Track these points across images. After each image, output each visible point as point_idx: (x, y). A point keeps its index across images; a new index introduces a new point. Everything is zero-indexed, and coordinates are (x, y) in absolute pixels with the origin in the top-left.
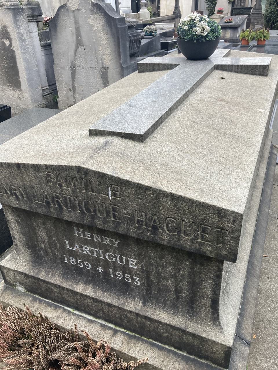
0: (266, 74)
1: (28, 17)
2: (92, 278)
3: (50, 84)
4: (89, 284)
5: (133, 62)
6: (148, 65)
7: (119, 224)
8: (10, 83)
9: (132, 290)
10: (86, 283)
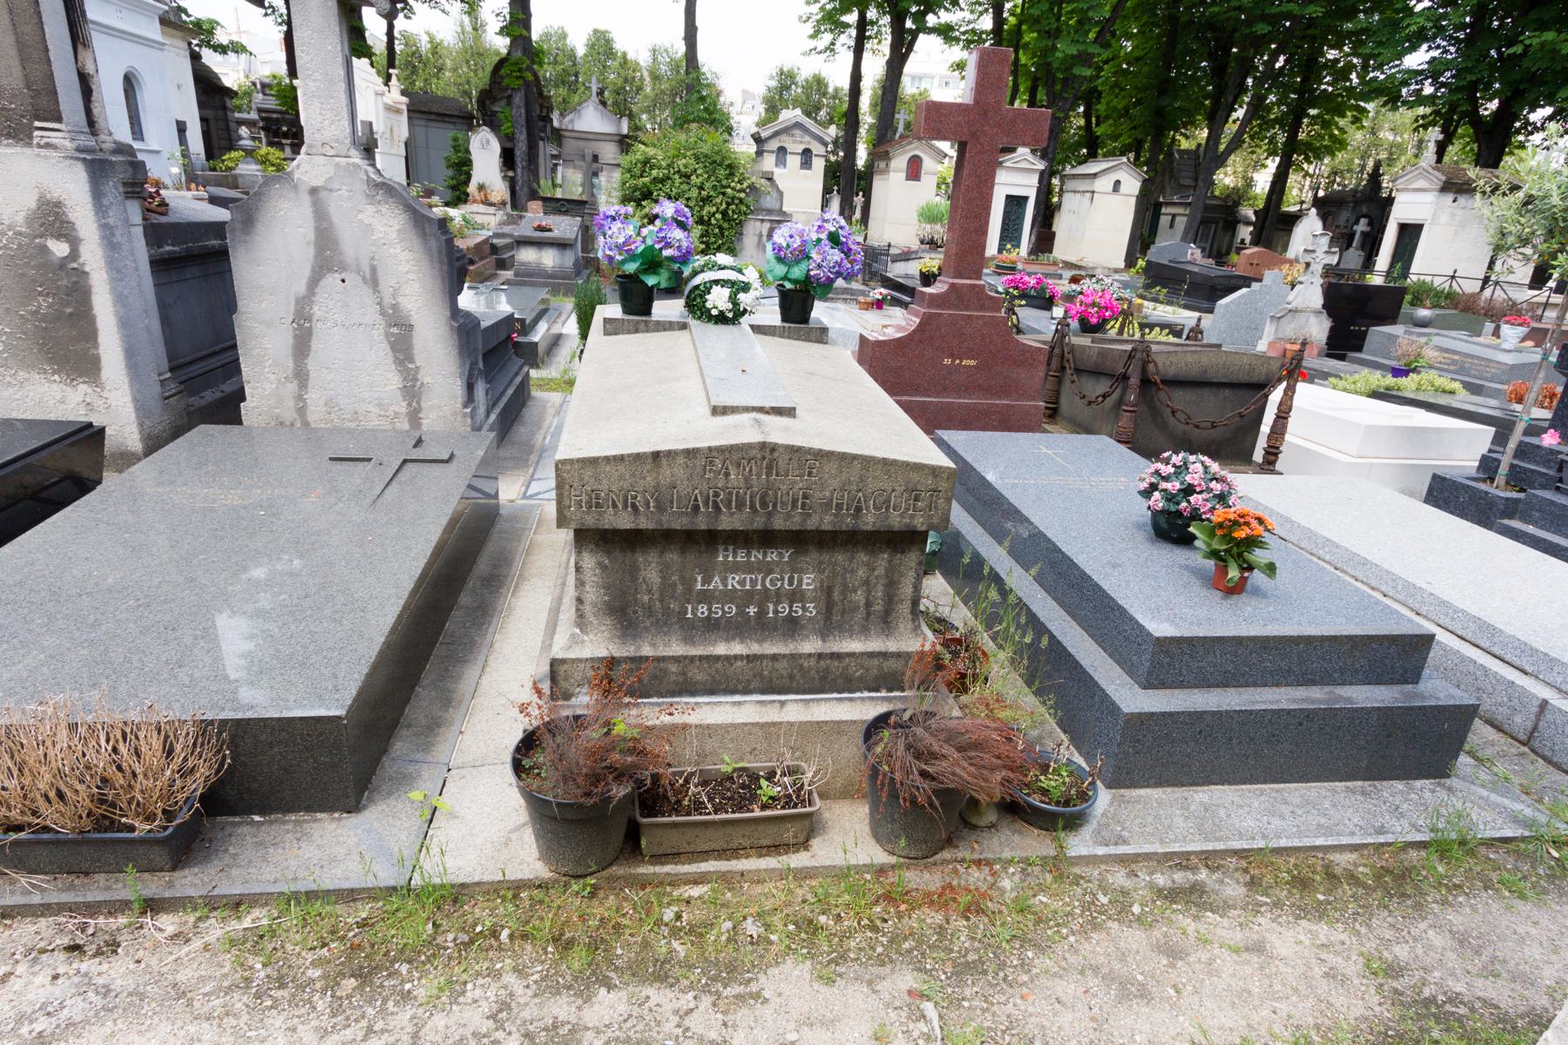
1: (125, 184)
2: (738, 628)
3: (175, 363)
4: (733, 639)
7: (809, 515)
8: (51, 361)
9: (803, 627)
10: (727, 640)
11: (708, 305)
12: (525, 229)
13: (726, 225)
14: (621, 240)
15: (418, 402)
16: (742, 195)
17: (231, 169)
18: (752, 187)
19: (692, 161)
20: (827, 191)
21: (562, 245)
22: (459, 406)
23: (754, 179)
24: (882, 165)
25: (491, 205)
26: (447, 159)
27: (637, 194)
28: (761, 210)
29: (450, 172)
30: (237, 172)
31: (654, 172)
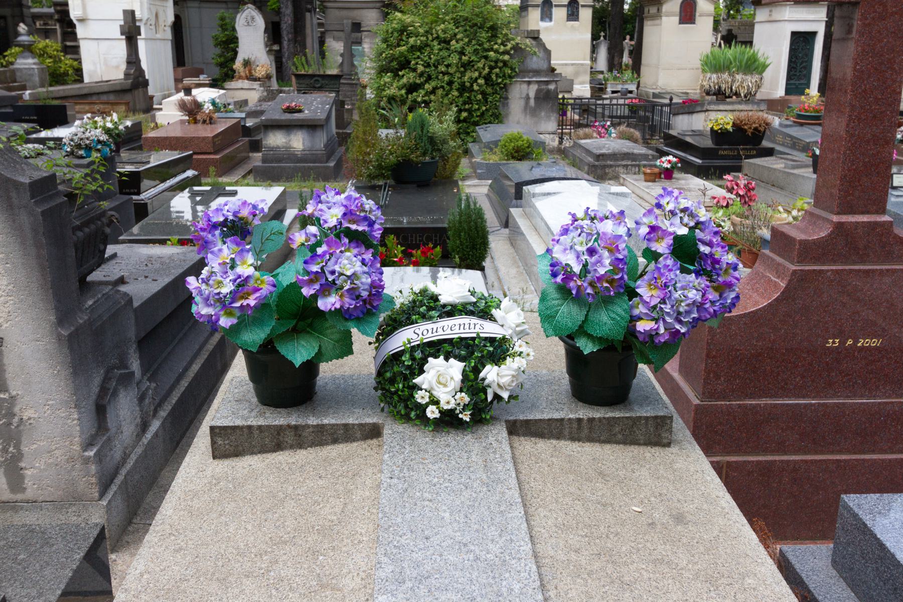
0: (665, 441)
5: (90, 303)
6: (256, 432)
11: (421, 397)
12: (274, 111)
13: (489, 90)
14: (227, 288)
15: (17, 446)
16: (506, 57)
17: (12, 63)
18: (516, 48)
19: (451, 26)
20: (595, 37)
21: (311, 126)
22: (77, 447)
23: (518, 39)
24: (653, 10)
25: (256, 80)
26: (216, 38)
27: (395, 63)
28: (525, 72)
29: (218, 51)
30: (16, 66)
31: (412, 41)
